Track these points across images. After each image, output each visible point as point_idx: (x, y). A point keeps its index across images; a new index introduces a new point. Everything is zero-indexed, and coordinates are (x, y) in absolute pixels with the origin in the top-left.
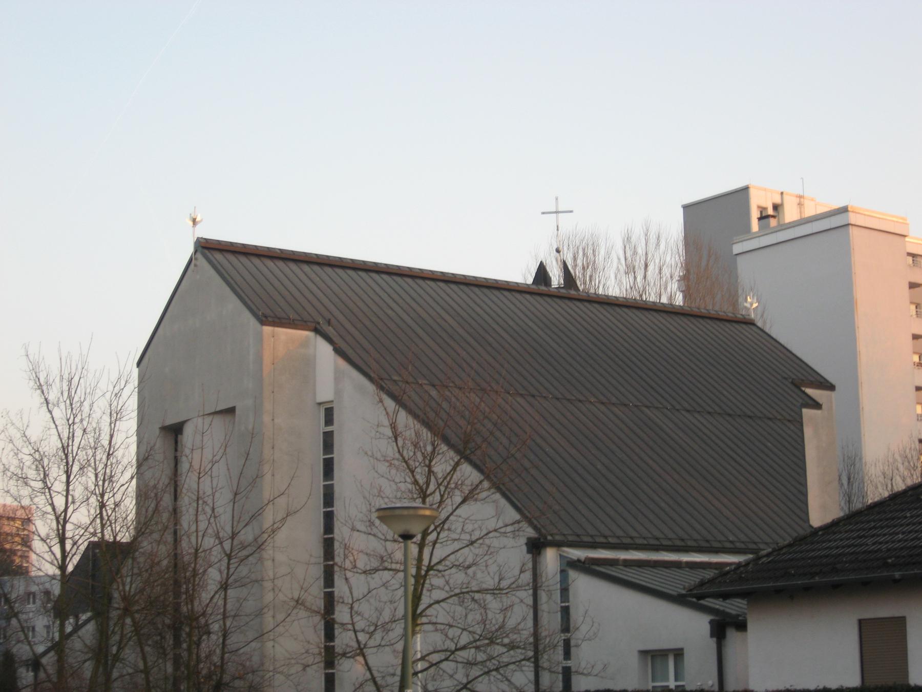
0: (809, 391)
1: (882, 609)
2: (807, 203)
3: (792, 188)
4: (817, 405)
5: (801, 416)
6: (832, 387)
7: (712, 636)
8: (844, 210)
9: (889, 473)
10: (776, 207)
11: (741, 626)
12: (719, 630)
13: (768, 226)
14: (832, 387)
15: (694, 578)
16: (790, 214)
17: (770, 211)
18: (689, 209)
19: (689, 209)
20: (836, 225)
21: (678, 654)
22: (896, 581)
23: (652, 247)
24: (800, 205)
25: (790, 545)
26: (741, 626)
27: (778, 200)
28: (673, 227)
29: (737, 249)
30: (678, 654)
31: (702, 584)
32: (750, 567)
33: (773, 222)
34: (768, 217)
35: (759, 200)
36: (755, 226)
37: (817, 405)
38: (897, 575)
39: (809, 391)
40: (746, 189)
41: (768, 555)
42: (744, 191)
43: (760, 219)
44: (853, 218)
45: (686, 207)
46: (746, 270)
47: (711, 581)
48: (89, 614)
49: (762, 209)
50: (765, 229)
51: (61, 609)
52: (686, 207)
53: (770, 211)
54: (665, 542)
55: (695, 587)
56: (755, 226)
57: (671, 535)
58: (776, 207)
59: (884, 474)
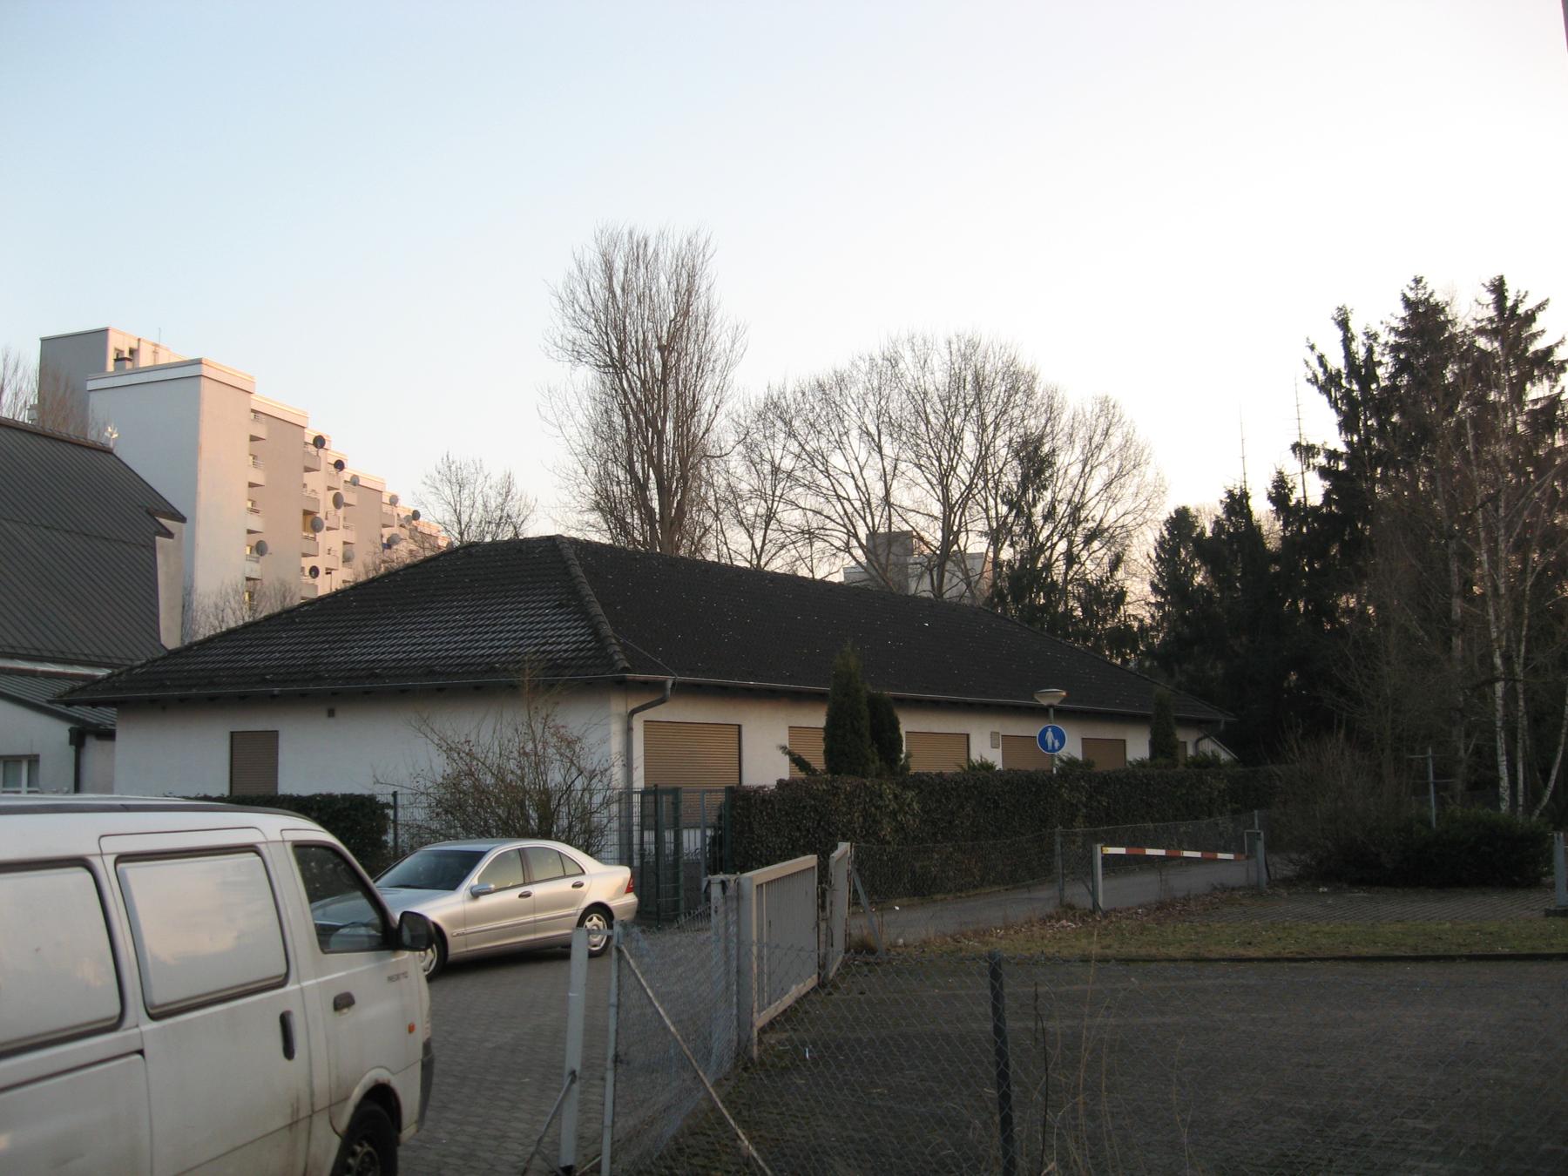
0: (162, 521)
1: (257, 723)
2: (161, 351)
3: (149, 336)
4: (169, 535)
5: (154, 542)
6: (183, 519)
7: (71, 743)
8: (198, 362)
9: (221, 604)
10: (132, 352)
11: (109, 735)
12: (78, 739)
13: (123, 368)
14: (183, 519)
15: (66, 686)
16: (145, 360)
17: (126, 355)
18: (50, 345)
19: (50, 345)
20: (189, 374)
21: (33, 760)
22: (273, 697)
23: (9, 373)
24: (155, 352)
25: (163, 658)
26: (109, 735)
27: (135, 346)
28: (32, 359)
29: (91, 385)
30: (33, 760)
31: (73, 691)
32: (123, 677)
33: (129, 365)
34: (124, 359)
35: (116, 343)
36: (110, 366)
37: (169, 535)
38: (276, 690)
39: (162, 521)
40: (105, 331)
41: (142, 666)
42: (103, 333)
43: (117, 360)
44: (205, 371)
45: (43, 340)
46: (99, 406)
47: (82, 689)
48: (863, 560)
49: (119, 352)
50: (120, 371)
51: (1229, 519)
52: (43, 340)
53: (126, 355)
54: (21, 651)
55: (66, 694)
56: (110, 366)
57: (26, 644)
58: (132, 352)
59: (216, 606)
